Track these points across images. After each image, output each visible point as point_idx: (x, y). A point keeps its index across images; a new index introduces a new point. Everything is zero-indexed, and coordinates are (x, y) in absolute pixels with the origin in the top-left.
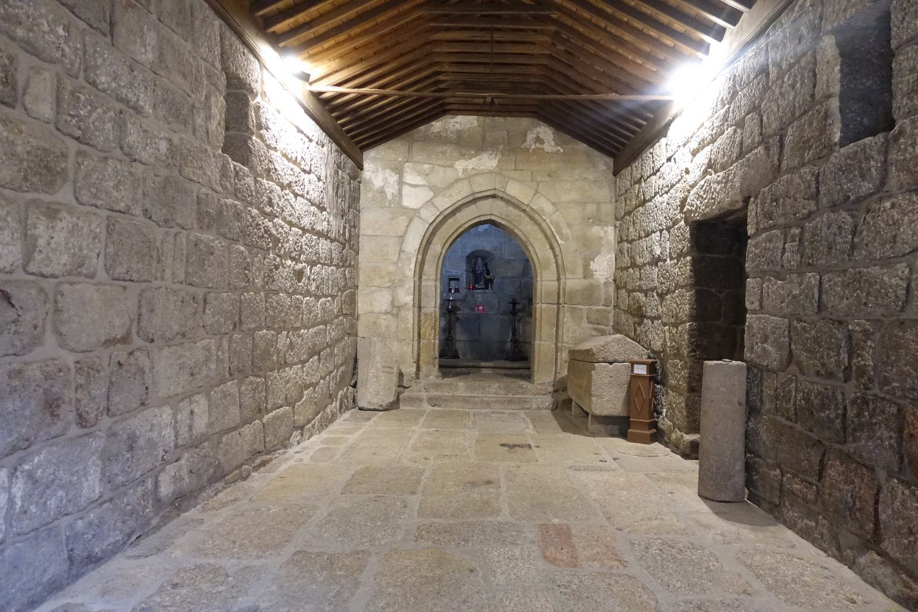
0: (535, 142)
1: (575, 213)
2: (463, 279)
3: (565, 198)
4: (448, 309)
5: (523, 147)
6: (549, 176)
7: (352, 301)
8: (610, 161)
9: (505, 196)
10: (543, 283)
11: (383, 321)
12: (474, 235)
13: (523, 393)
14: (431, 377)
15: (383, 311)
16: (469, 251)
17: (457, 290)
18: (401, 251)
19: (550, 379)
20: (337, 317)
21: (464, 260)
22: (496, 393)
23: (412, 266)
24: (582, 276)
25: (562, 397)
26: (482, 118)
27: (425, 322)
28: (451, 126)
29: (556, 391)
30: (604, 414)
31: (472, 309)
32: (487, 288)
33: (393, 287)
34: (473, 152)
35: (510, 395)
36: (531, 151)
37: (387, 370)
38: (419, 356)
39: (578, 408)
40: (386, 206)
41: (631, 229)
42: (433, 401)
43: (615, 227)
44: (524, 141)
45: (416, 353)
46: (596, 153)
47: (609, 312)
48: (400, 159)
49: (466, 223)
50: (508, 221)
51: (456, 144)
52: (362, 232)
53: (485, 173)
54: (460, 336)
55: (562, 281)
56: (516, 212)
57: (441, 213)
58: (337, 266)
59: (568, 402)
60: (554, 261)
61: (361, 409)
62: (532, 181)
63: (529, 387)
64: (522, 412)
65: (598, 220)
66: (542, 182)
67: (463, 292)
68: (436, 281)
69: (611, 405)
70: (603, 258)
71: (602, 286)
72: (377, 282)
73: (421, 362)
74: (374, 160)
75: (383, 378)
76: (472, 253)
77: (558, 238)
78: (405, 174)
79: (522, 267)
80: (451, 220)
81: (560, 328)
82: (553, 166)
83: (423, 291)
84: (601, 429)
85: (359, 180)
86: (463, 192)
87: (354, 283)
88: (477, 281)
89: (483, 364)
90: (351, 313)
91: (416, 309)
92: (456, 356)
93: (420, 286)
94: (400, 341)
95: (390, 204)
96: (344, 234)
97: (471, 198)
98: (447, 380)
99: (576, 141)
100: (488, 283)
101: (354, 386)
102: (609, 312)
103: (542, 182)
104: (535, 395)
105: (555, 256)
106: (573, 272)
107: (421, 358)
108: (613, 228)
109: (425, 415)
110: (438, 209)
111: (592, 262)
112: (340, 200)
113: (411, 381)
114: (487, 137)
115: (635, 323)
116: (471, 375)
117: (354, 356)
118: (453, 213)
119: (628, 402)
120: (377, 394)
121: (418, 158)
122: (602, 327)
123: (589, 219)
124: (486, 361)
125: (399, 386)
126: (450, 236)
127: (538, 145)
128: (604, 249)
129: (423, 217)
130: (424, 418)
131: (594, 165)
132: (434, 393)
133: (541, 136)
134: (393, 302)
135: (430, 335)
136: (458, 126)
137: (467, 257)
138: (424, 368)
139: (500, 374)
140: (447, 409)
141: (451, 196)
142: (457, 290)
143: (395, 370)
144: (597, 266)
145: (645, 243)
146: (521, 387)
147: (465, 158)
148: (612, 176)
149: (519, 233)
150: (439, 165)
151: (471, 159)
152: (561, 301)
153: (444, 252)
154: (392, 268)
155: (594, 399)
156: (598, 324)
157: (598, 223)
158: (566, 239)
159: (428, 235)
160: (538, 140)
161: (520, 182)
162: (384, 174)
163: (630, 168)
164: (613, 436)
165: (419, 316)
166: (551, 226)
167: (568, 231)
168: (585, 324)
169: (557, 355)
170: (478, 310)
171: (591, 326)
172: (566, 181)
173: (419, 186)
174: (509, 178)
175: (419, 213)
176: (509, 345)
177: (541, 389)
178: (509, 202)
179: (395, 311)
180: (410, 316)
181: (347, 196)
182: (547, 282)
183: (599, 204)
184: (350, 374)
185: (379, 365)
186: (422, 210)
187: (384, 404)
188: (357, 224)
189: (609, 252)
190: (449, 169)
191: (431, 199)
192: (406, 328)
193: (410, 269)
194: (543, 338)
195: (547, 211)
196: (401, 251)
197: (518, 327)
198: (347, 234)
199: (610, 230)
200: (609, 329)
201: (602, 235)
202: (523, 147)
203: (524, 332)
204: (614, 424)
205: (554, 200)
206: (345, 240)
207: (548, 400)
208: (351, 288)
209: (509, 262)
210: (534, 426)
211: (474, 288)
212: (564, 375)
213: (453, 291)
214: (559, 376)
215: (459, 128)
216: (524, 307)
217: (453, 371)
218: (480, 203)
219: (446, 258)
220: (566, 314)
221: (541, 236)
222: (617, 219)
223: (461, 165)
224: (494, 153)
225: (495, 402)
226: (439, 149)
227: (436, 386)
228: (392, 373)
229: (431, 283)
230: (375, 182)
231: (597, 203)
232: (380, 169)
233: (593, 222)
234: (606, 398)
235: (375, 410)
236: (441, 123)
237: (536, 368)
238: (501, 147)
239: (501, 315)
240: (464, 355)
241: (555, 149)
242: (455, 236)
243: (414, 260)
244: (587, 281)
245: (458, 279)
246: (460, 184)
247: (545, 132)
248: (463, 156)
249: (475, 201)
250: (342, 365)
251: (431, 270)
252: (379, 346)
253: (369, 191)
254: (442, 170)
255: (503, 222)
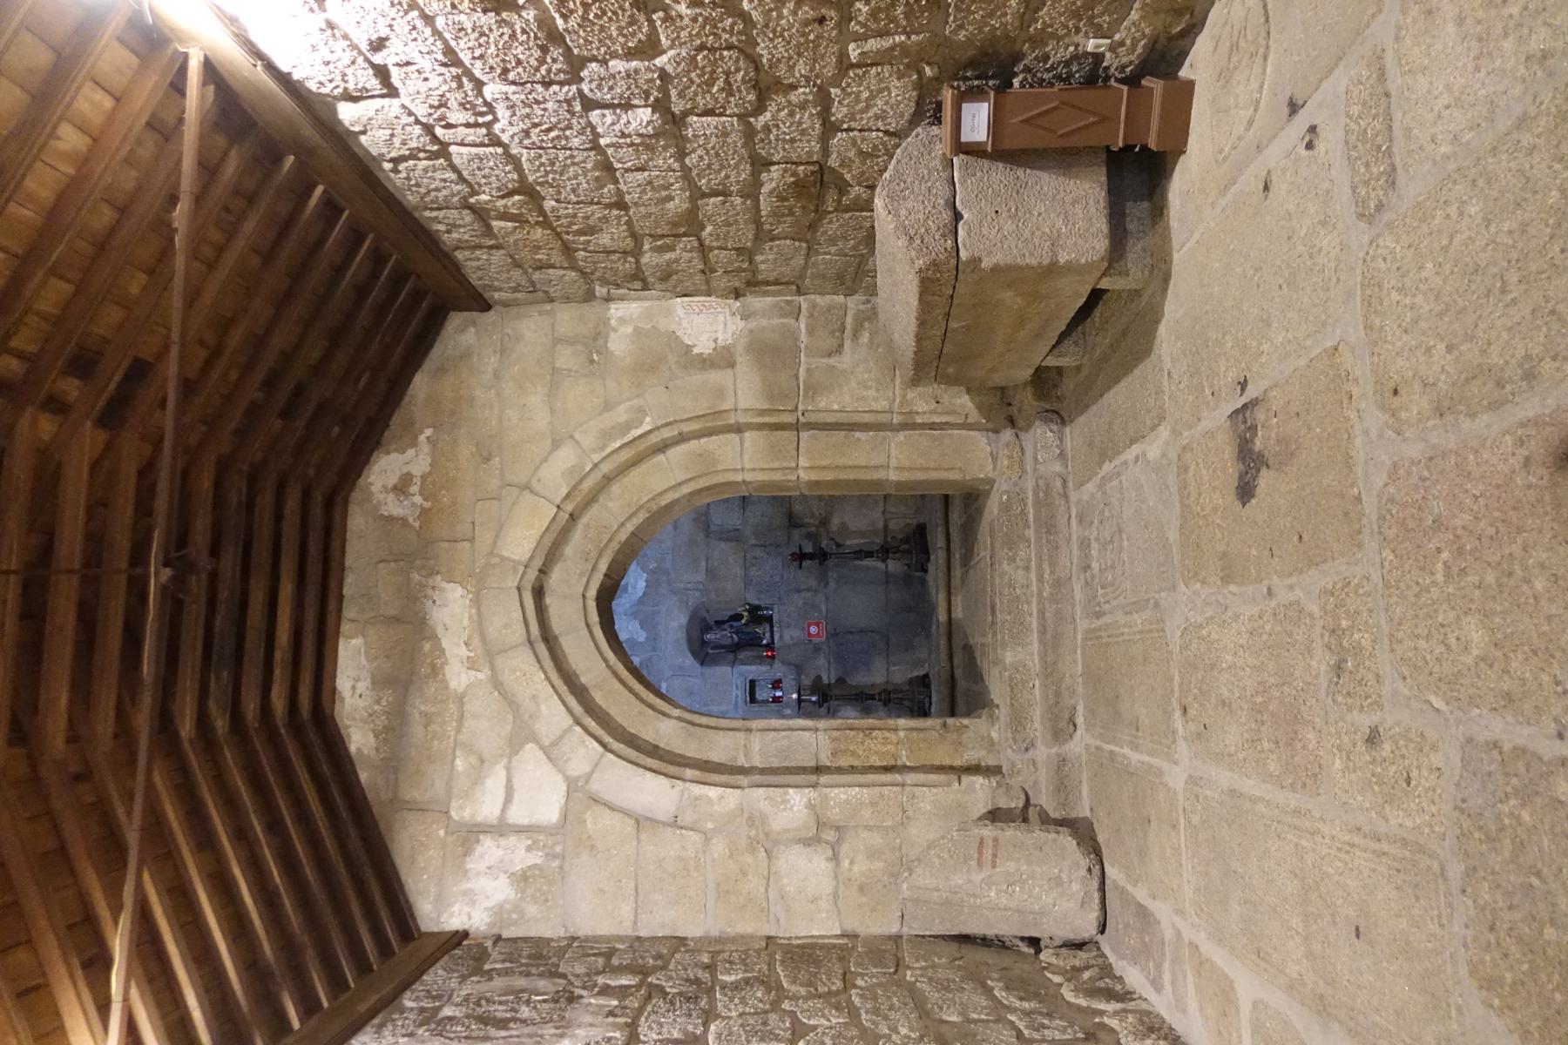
0: (407, 495)
1: (577, 395)
2: (753, 671)
3: (541, 421)
4: (819, 704)
5: (417, 524)
6: (487, 459)
7: (805, 955)
8: (455, 320)
9: (538, 563)
10: (748, 466)
11: (857, 866)
12: (655, 649)
13: (1023, 502)
14: (994, 735)
15: (831, 866)
16: (689, 661)
17: (776, 684)
18: (675, 823)
19: (980, 441)
20: (853, 1013)
21: (708, 671)
22: (1027, 569)
23: (713, 792)
24: (729, 371)
25: (1027, 400)
26: (346, 627)
27: (853, 753)
28: (361, 703)
29: (1012, 422)
30: (1105, 228)
31: (817, 649)
32: (769, 619)
33: (767, 843)
34: (427, 647)
35: (1031, 533)
36: (427, 505)
37: (988, 853)
38: (940, 769)
39: (1062, 347)
40: (561, 868)
41: (605, 239)
42: (1061, 728)
43: (608, 299)
44: (403, 522)
45: (933, 777)
46: (437, 352)
47: (814, 306)
48: (442, 833)
49: (605, 660)
50: (600, 556)
51: (406, 690)
52: (626, 930)
53: (479, 614)
54: (876, 675)
55: (742, 419)
56: (577, 536)
57: (578, 722)
58: (709, 1016)
59: (1044, 381)
60: (694, 443)
61: (1102, 929)
62: (498, 499)
63: (1005, 487)
64: (1073, 496)
65: (595, 340)
66: (502, 475)
67: (778, 670)
68: (749, 730)
69: (1078, 209)
70: (684, 324)
71: (752, 324)
72: (755, 884)
73: (957, 763)
74: (441, 901)
75: (1011, 866)
76: (694, 653)
77: (639, 432)
78: (479, 819)
79: (723, 544)
80: (599, 697)
81: (858, 418)
82: (466, 450)
83: (775, 763)
84: (1139, 247)
85: (489, 944)
86: (525, 667)
87: (758, 952)
88: (752, 642)
89: (942, 617)
90: (841, 959)
91: (823, 779)
92: (924, 681)
93: (763, 771)
94: (906, 818)
95: (555, 857)
96: (622, 992)
97: (542, 649)
98: (997, 690)
99: (406, 400)
100: (758, 615)
101: (1034, 942)
102: (814, 306)
103: (502, 475)
104: (1024, 472)
105: (682, 439)
106: (720, 393)
107: (947, 762)
108: (613, 306)
109: (1108, 747)
110: (569, 729)
111: (696, 351)
112: (525, 1012)
113: (1009, 788)
114: (392, 613)
115: (841, 209)
116: (971, 641)
117: (954, 946)
118: (579, 691)
119: (1062, 158)
120: (1056, 881)
121: (439, 788)
122: (849, 320)
123: (592, 361)
124: (932, 609)
125: (1025, 820)
126: (637, 696)
127: (414, 489)
128: (663, 324)
129: (588, 769)
130: (1126, 751)
131: (466, 355)
132: (1037, 725)
133: (393, 480)
134: (808, 842)
135: (886, 741)
136: (362, 686)
137: (702, 664)
138: (972, 755)
139: (963, 580)
140: (1080, 689)
141: (534, 697)
142: (776, 684)
143: (988, 831)
144: (704, 338)
145: (630, 177)
146: (1006, 508)
147: (442, 667)
148: (492, 312)
149: (630, 527)
150: (458, 730)
151: (443, 651)
152: (789, 419)
153: (677, 712)
154: (719, 847)
155: (1063, 258)
156: (843, 329)
157: (601, 341)
158: (641, 412)
159: (632, 754)
160: (401, 488)
161: (501, 527)
162: (478, 873)
163: (459, 255)
164: (1158, 211)
165: (839, 770)
166: (608, 450)
167: (622, 408)
168: (846, 360)
169: (923, 426)
170: (818, 635)
171: (847, 344)
172: (500, 420)
173: (509, 781)
174: (491, 554)
175: (577, 779)
176: (894, 566)
177: (1010, 457)
178: (551, 554)
179: (830, 835)
180: (841, 796)
181: (521, 982)
182: (746, 457)
183: (557, 341)
184: (1006, 959)
185: (978, 877)
186: (569, 773)
187: (1084, 862)
188: (604, 947)
189: (669, 312)
190: (468, 707)
191: (542, 748)
192: (873, 804)
193: (721, 798)
194: (882, 460)
195: (572, 461)
196: (675, 823)
197: (851, 546)
198: (625, 981)
199: (617, 310)
200: (854, 303)
201: (629, 330)
202: (417, 524)
203: (861, 534)
204: (1124, 215)
205: (549, 442)
206: (638, 987)
207: (1041, 435)
208: (771, 965)
209: (711, 573)
210: (1132, 442)
211: (770, 647)
212: (970, 405)
213: (779, 694)
214: (975, 416)
215: (368, 682)
216: (809, 536)
217: (962, 684)
218: (557, 625)
219: (697, 711)
220: (822, 405)
221: (634, 476)
222: (589, 296)
223: (458, 676)
224: (430, 592)
225: (1053, 565)
226: (417, 732)
227: (1018, 721)
228: (996, 840)
229: (756, 742)
230: (498, 897)
231: (554, 345)
232: (465, 886)
233: (599, 353)
234: (1060, 224)
235: (1102, 888)
236: (352, 730)
237: (954, 476)
238: (416, 577)
239: (827, 584)
240: (920, 663)
241: (425, 448)
242: (651, 698)
243: (698, 790)
244: (739, 360)
245: (752, 683)
246: (507, 677)
247: (383, 471)
248: (436, 671)
249: (549, 638)
250: (988, 991)
251: (722, 746)
252: (924, 878)
253: (522, 914)
254: (469, 723)
255: (603, 567)
